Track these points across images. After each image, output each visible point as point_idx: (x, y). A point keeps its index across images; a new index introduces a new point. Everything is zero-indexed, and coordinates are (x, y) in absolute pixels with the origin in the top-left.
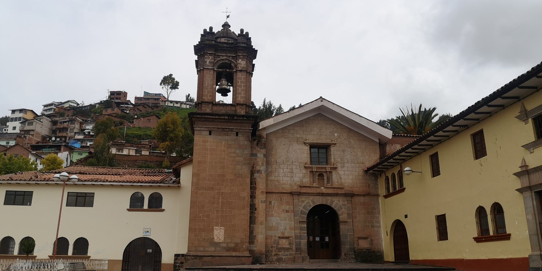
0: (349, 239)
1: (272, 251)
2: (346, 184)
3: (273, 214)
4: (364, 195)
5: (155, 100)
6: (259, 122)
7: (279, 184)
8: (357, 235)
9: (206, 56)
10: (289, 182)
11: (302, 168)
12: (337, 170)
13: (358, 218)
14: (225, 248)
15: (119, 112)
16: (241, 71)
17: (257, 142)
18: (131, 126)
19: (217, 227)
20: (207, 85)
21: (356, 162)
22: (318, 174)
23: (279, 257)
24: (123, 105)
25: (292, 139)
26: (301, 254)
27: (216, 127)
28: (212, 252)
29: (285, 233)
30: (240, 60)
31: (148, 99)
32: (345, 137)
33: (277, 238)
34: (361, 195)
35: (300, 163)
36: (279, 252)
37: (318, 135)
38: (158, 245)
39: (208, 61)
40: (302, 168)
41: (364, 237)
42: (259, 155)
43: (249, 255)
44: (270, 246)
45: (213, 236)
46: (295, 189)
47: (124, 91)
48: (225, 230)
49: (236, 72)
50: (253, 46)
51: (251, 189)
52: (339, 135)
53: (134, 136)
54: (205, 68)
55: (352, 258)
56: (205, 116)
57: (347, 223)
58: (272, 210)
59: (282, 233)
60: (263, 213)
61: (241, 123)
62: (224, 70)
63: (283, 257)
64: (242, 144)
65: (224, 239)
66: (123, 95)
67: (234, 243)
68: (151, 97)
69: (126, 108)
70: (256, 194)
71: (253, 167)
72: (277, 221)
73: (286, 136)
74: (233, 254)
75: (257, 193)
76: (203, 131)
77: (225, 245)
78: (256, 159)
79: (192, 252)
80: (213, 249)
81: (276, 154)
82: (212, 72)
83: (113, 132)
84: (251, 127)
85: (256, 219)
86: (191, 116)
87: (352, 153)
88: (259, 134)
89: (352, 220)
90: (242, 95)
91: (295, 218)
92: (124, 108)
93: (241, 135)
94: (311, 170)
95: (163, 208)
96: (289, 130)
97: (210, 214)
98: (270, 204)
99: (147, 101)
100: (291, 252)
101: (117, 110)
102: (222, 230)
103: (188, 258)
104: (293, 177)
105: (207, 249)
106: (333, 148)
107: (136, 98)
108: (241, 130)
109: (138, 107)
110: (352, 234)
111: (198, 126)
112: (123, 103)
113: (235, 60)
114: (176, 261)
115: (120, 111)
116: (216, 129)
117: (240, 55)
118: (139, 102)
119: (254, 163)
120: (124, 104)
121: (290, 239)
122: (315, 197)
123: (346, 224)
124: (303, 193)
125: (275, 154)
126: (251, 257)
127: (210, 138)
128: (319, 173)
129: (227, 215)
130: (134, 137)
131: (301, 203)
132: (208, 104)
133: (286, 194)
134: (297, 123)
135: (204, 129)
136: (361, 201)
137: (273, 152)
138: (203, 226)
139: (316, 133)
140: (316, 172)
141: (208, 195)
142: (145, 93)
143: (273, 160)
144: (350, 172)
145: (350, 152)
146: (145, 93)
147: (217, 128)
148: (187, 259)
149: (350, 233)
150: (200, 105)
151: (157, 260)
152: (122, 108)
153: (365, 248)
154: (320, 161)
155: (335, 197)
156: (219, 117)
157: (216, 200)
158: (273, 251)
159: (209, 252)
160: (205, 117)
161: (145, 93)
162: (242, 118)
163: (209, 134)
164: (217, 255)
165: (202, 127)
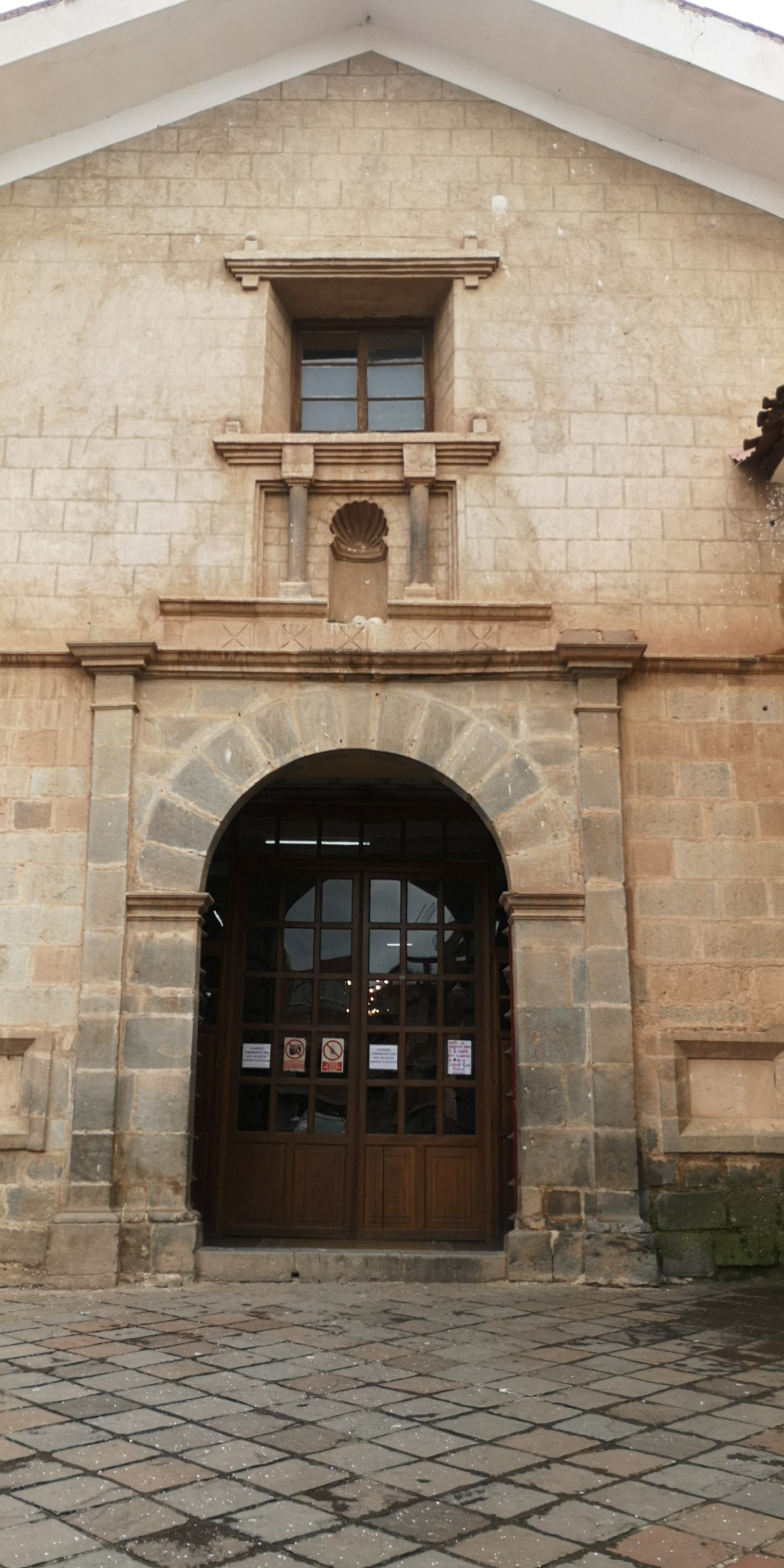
0: (588, 1057)
2: (577, 584)
4: (741, 661)
8: (670, 1023)
11: (198, 463)
12: (498, 466)
13: (678, 866)
21: (667, 401)
22: (331, 506)
25: (122, 246)
26: (115, 1197)
32: (571, 219)
34: (714, 671)
35: (176, 420)
37: (352, 208)
40: (198, 463)
41: (742, 1037)
52: (520, 204)
55: (612, 1243)
57: (579, 913)
73: (79, 221)
87: (636, 333)
89: (620, 886)
91: (125, 795)
94: (267, 474)
96: (108, 179)
100: (29, 1183)
104: (107, 533)
106: (472, 297)
110: (619, 1012)
121: (34, 1062)
122: (291, 694)
123: (566, 919)
124: (183, 656)
128: (342, 501)
131: (168, 744)
133: (36, 672)
134: (176, 127)
136: (712, 719)
139: (329, 193)
140: (314, 488)
144: (616, 482)
145: (613, 329)
149: (594, 1005)
153: (749, 1139)
154: (371, 394)
155: (471, 687)
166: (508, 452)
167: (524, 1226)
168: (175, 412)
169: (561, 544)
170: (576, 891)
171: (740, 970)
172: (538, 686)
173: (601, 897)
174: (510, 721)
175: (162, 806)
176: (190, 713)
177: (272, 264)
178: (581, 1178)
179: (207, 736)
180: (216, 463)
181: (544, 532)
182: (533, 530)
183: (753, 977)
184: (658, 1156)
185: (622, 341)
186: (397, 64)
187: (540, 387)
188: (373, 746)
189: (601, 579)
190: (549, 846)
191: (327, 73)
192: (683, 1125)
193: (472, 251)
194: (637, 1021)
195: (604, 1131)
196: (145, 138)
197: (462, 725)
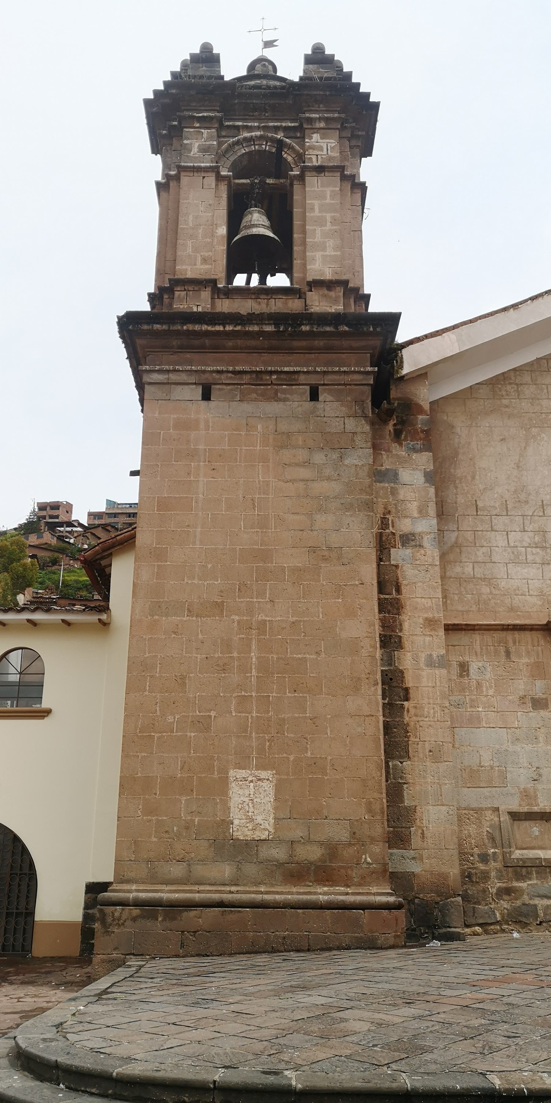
1: (485, 876)
3: (479, 719)
5: (130, 517)
6: (401, 350)
7: (495, 592)
9: (185, 129)
10: (535, 584)
14: (280, 865)
15: (54, 541)
16: (320, 170)
17: (395, 425)
18: (76, 566)
19: (242, 773)
20: (191, 225)
23: (519, 903)
24: (63, 528)
27: (231, 369)
28: (224, 885)
29: (536, 796)
30: (316, 137)
31: (115, 515)
33: (505, 818)
36: (518, 880)
38: (24, 849)
39: (197, 145)
42: (405, 475)
43: (392, 899)
44: (476, 850)
45: (227, 809)
47: (66, 502)
48: (276, 785)
49: (301, 178)
50: (358, 85)
51: (380, 611)
53: (80, 585)
54: (186, 169)
56: (184, 323)
58: (472, 700)
59: (526, 795)
60: (438, 708)
61: (329, 349)
62: (256, 181)
63: (537, 901)
64: (333, 430)
65: (275, 824)
66: (65, 510)
67: (321, 844)
68: (120, 512)
69: (68, 534)
70: (401, 630)
71: (384, 523)
72: (497, 747)
74: (315, 893)
75: (406, 626)
76: (180, 388)
77: (279, 853)
78: (394, 492)
79: (134, 887)
80: (227, 870)
81: (473, 478)
82: (211, 180)
83: (25, 570)
84: (369, 364)
85: (408, 737)
86: (131, 327)
88: (399, 395)
90: (327, 253)
92: (65, 534)
93: (329, 398)
95: (45, 704)
96: (517, 384)
97: (213, 714)
98: (461, 676)
99: (112, 520)
101: (48, 538)
102: (265, 784)
103: (117, 914)
105: (200, 871)
107: (90, 514)
108: (328, 379)
109: (92, 531)
111: (157, 368)
112: (61, 524)
113: (296, 140)
114: (90, 911)
115: (55, 539)
116: (230, 375)
117: (316, 118)
118: (97, 522)
119: (385, 508)
120: (65, 526)
125: (469, 478)
126: (398, 907)
129: (284, 719)
130: (79, 589)
132: (196, 288)
135: (183, 377)
137: (458, 471)
138: (182, 768)
141: (200, 636)
142: (110, 503)
143: (461, 500)
146: (109, 502)
147: (234, 372)
148: (109, 920)
150: (166, 296)
151: (17, 909)
152: (61, 534)
156: (238, 328)
157: (235, 654)
158: (493, 874)
159: (210, 884)
160: (185, 327)
161: (109, 502)
162: (329, 325)
163: (200, 399)
164: (245, 897)
165: (175, 371)
196: (531, 364)
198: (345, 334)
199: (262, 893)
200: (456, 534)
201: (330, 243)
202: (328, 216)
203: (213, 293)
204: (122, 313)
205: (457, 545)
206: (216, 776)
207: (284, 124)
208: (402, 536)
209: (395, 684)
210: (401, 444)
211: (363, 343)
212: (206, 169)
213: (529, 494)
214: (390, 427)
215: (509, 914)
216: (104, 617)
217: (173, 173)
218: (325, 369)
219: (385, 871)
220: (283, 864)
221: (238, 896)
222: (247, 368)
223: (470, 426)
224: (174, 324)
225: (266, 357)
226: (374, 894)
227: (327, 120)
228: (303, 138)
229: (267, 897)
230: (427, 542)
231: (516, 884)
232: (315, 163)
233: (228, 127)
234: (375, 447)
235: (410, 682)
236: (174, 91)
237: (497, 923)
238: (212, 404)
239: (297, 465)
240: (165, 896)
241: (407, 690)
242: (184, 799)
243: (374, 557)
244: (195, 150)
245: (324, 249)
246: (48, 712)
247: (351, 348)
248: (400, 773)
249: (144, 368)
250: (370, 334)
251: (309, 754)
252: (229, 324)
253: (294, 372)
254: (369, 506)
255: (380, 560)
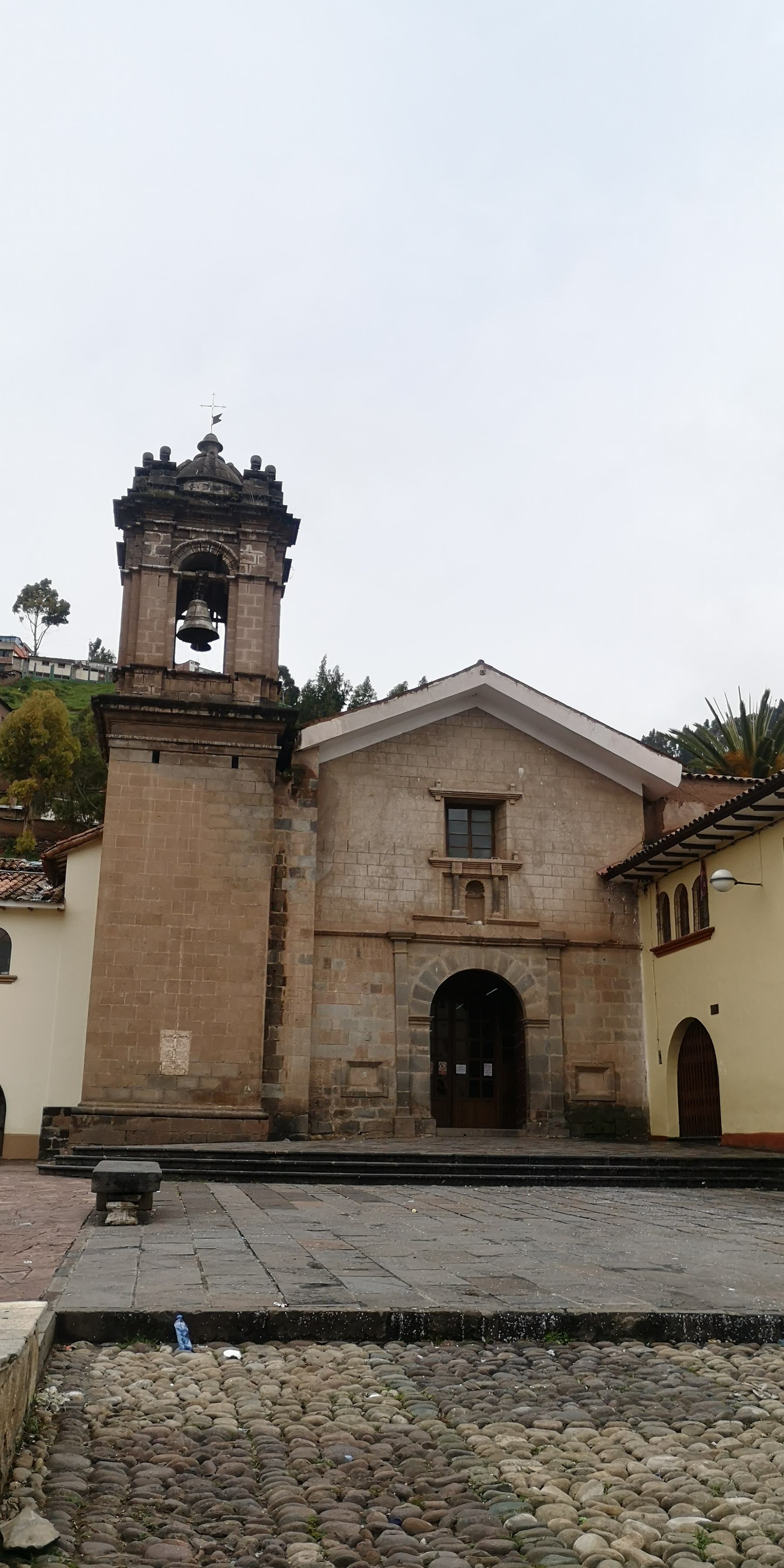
1: (328, 1103)
2: (547, 914)
7: (354, 908)
10: (383, 904)
12: (520, 871)
14: (191, 1091)
16: (250, 578)
19: (169, 1032)
22: (467, 881)
23: (348, 1120)
27: (175, 740)
33: (344, 1065)
41: (594, 1065)
43: (261, 1114)
44: (323, 1086)
45: (158, 1055)
46: (401, 924)
52: (528, 772)
54: (146, 568)
59: (361, 1051)
60: (304, 992)
63: (359, 1119)
67: (219, 1078)
70: (285, 937)
71: (279, 859)
73: (377, 770)
77: (192, 1084)
78: (288, 836)
79: (95, 1103)
80: (157, 1094)
81: (348, 824)
82: (165, 578)
84: (276, 742)
88: (297, 762)
93: (246, 766)
94: (446, 871)
95: (12, 972)
98: (325, 968)
100: (384, 1107)
102: (184, 1040)
105: (138, 1094)
108: (246, 752)
117: (249, 533)
121: (382, 1070)
122: (457, 949)
124: (423, 936)
125: (345, 824)
126: (266, 1118)
127: (156, 773)
128: (470, 880)
131: (417, 965)
135: (139, 744)
136: (588, 962)
139: (463, 764)
143: (337, 839)
147: (177, 743)
150: (127, 674)
153: (595, 1096)
155: (513, 949)
156: (182, 712)
157: (168, 952)
158: (333, 1102)
162: (248, 714)
165: (133, 739)
166: (525, 866)
167: (530, 1121)
168: (414, 846)
169: (541, 900)
170: (547, 1019)
171: (595, 1045)
172: (534, 950)
173: (554, 1021)
174: (526, 961)
175: (417, 987)
176: (423, 955)
177: (445, 793)
178: (547, 1107)
179: (429, 963)
180: (429, 866)
181: (536, 895)
182: (532, 894)
183: (598, 1047)
184: (569, 1101)
185: (562, 826)
186: (486, 713)
187: (535, 842)
188: (483, 968)
189: (554, 913)
190: (538, 1003)
191: (462, 715)
192: (577, 1092)
193: (513, 792)
194: (565, 1060)
195: (554, 1094)
196: (398, 737)
197: (511, 962)
198: (259, 720)
199: (178, 1108)
200: (331, 865)
201: (254, 642)
202: (254, 618)
203: (163, 674)
204: (71, 610)
205: (332, 873)
206: (151, 1033)
207: (224, 532)
208: (290, 869)
209: (277, 974)
210: (295, 801)
211: (272, 727)
212: (162, 570)
213: (385, 838)
214: (289, 787)
215: (340, 1128)
216: (62, 907)
217: (135, 568)
218: (244, 745)
219: (259, 1096)
220: (193, 1091)
221: (163, 1110)
222: (186, 741)
223: (349, 784)
224: (134, 705)
225: (201, 731)
226: (251, 1110)
227: (258, 534)
228: (239, 543)
229: (181, 1111)
230: (308, 875)
231: (347, 1108)
232: (247, 573)
233: (181, 530)
234: (276, 801)
235: (287, 973)
236: (139, 501)
237: (332, 1133)
238: (160, 766)
239: (218, 816)
240: (116, 1109)
241: (285, 978)
242: (129, 1048)
243: (269, 887)
244: (154, 551)
245: (250, 647)
246: (15, 979)
247: (263, 729)
248: (276, 1034)
249: (110, 736)
250: (276, 722)
251: (215, 1021)
252: (175, 708)
253: (221, 746)
254: (268, 849)
255: (273, 886)
